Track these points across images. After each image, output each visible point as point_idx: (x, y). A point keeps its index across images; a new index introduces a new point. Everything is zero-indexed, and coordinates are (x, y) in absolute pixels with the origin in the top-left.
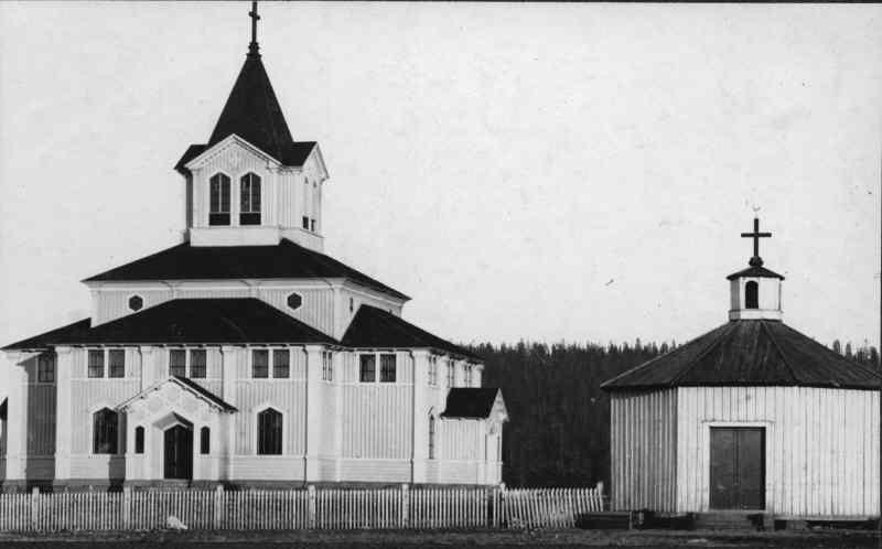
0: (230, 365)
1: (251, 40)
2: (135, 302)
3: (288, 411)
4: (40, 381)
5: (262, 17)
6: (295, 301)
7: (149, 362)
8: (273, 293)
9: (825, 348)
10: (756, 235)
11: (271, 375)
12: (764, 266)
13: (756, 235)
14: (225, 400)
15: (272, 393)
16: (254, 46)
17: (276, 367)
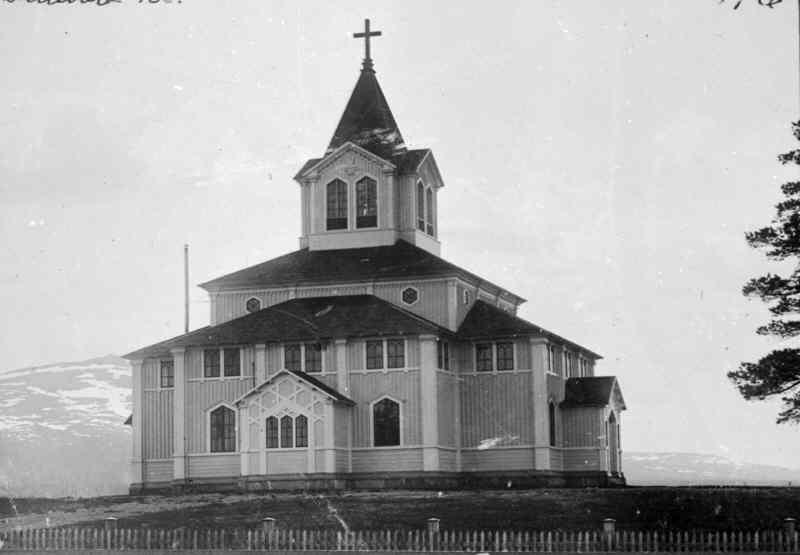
0: (342, 362)
1: (364, 56)
2: (252, 304)
3: (404, 402)
4: (206, 376)
5: (780, 187)
6: (410, 296)
7: (261, 361)
8: (391, 293)
9: (247, 316)
10: (368, 34)
11: (222, 373)
12: (36, 2)
13: (368, 34)
14: (341, 392)
15: (384, 384)
16: (368, 63)
17: (226, 366)
